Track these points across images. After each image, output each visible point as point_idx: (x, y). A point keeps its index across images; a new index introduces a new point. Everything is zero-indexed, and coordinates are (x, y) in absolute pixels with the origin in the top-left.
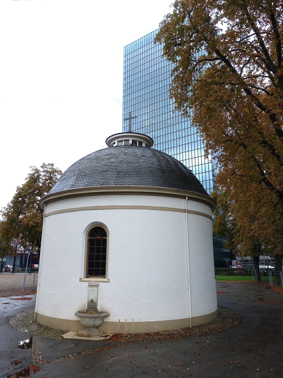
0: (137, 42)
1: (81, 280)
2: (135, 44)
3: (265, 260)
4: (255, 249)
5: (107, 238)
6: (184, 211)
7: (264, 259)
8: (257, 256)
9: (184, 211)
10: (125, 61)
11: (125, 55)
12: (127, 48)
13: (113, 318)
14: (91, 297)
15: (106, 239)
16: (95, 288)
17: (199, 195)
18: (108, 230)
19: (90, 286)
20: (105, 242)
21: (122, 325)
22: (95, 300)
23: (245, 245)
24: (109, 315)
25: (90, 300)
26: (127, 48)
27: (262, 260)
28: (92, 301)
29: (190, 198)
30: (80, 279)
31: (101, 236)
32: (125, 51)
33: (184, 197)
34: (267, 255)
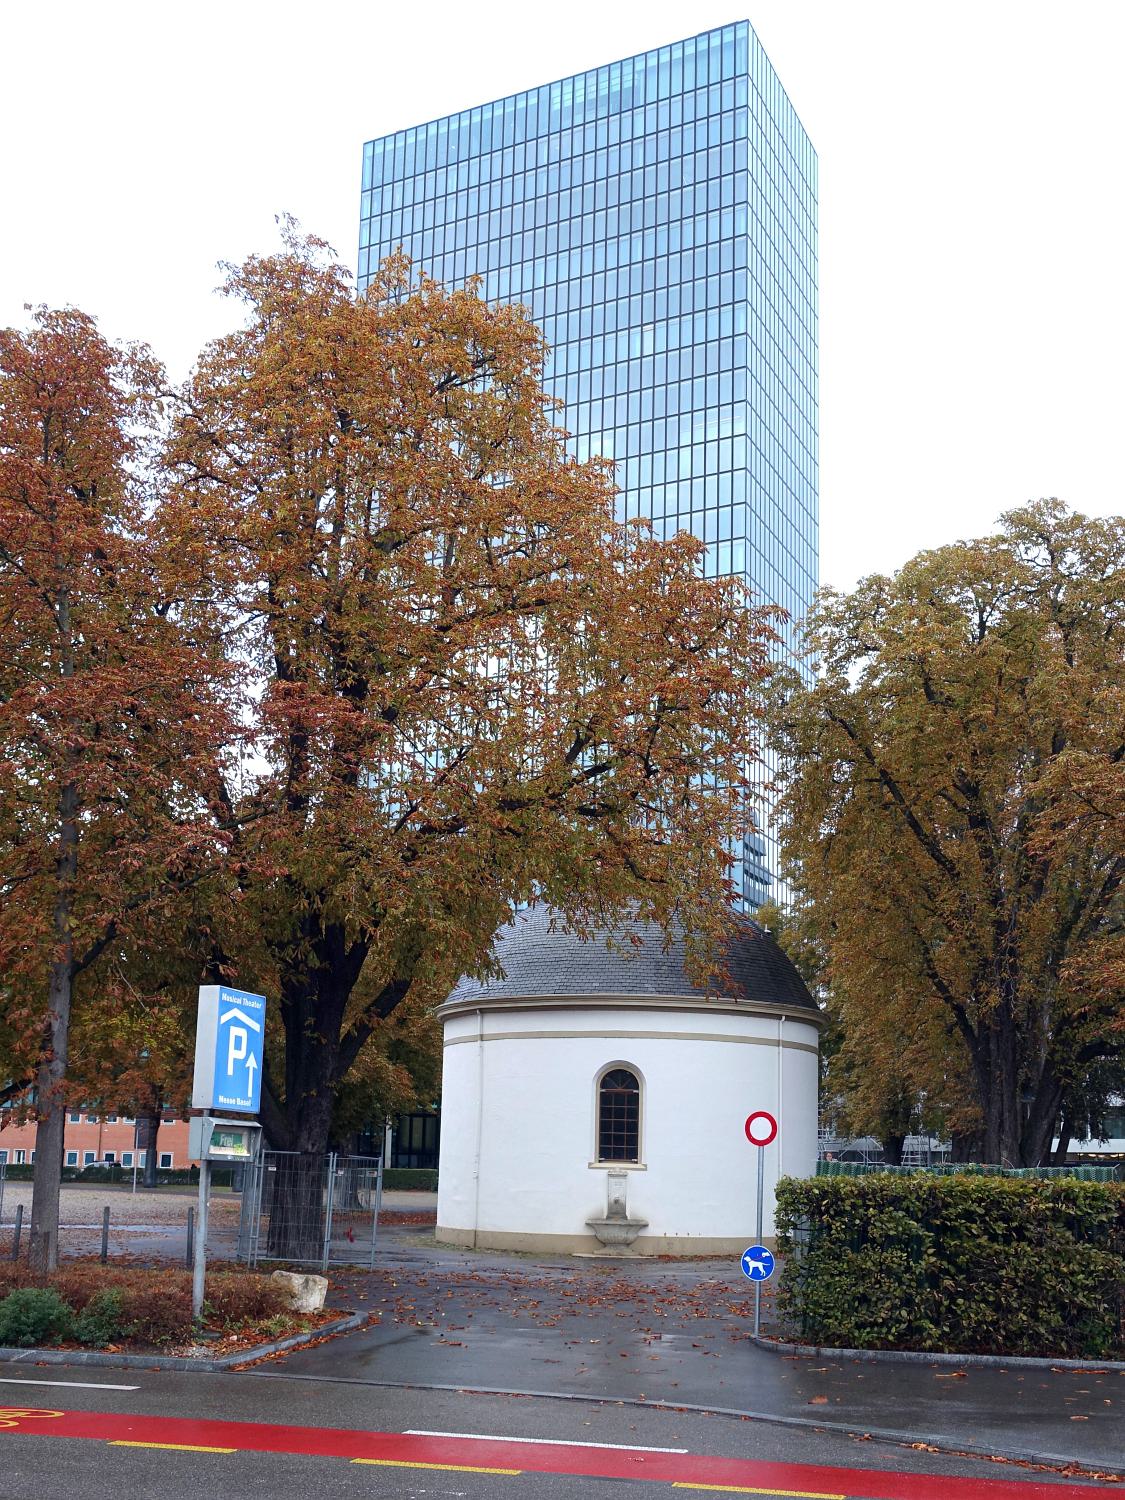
0: (432, 129)
1: (590, 1166)
2: (419, 138)
3: (925, 1153)
4: (893, 1113)
5: (600, 1090)
6: (777, 1043)
7: (919, 1149)
8: (898, 1134)
9: (777, 1043)
10: (367, 214)
11: (368, 187)
12: (379, 149)
13: (654, 1231)
14: (614, 1196)
15: (602, 1087)
16: (622, 1180)
17: (804, 1012)
18: (642, 1077)
19: (610, 1175)
20: (634, 1100)
21: (670, 1241)
22: (622, 1200)
23: (865, 1099)
24: (646, 1226)
25: (612, 1201)
26: (379, 149)
27: (912, 1153)
28: (616, 1202)
29: (788, 1018)
30: (590, 1164)
31: (627, 1087)
32: (368, 163)
33: (779, 1017)
34: (931, 1135)
